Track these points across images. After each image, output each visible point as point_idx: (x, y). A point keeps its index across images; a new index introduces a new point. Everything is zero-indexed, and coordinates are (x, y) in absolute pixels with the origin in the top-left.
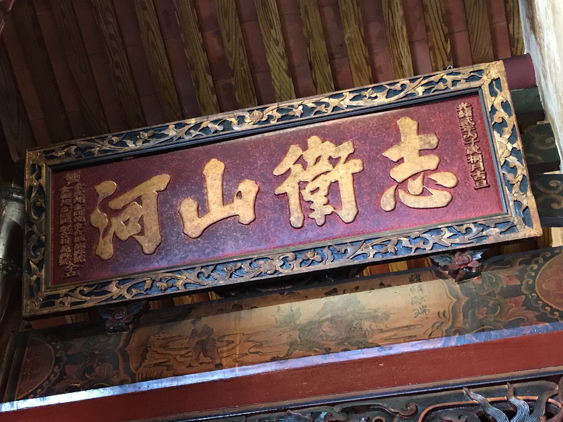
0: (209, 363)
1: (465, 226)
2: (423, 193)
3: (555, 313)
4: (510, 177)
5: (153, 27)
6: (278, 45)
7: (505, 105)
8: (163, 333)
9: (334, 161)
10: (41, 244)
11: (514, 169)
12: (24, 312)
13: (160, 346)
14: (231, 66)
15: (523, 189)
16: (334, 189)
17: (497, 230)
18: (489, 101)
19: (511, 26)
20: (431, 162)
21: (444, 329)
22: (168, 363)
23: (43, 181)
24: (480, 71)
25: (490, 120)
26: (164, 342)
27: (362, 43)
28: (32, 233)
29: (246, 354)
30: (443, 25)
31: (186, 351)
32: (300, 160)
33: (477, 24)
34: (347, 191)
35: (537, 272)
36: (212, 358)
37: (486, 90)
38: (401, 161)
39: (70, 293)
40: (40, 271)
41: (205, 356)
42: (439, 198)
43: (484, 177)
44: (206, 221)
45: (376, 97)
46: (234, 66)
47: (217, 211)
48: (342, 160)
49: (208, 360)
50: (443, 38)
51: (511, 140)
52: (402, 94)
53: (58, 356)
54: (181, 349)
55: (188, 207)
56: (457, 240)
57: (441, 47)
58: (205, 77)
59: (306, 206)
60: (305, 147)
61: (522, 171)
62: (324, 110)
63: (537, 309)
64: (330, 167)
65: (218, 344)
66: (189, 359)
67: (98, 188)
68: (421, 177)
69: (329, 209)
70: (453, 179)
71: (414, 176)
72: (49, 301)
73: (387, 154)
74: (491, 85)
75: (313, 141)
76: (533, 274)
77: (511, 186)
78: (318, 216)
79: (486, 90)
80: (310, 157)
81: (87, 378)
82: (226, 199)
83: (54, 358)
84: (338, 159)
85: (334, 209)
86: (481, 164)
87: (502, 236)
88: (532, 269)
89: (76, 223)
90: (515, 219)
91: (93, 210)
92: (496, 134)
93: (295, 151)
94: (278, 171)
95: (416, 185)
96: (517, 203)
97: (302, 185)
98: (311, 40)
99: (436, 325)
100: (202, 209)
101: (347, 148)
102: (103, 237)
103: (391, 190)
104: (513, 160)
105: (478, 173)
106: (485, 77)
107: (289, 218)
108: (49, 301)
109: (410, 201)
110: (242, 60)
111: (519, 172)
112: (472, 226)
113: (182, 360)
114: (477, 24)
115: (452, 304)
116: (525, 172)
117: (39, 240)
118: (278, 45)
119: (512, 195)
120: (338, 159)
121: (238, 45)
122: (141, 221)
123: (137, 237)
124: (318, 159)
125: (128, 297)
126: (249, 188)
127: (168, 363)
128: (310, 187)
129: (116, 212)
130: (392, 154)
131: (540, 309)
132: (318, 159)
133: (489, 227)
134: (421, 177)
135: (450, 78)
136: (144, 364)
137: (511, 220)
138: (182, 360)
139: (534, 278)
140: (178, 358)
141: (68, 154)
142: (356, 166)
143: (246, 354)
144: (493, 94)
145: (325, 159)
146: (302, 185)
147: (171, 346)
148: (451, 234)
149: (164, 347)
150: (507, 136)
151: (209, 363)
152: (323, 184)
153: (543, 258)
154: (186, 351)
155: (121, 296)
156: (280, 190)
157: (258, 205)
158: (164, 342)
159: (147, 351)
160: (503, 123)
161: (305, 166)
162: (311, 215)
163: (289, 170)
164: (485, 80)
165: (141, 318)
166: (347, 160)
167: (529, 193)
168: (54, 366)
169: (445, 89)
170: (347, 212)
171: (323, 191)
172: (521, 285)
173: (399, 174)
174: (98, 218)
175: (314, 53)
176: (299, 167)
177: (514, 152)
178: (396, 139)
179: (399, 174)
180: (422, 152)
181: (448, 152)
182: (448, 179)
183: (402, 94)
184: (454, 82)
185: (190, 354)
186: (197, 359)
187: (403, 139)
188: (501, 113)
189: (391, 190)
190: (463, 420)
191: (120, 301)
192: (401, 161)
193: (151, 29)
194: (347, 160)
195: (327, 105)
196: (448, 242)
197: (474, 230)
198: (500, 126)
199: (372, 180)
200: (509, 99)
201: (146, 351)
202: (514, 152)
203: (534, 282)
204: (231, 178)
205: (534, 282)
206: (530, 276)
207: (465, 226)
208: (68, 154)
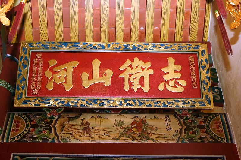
0: (88, 136)
1: (188, 101)
2: (175, 86)
3: (216, 137)
4: (205, 86)
5: (75, 3)
6: (121, 19)
7: (206, 60)
8: (70, 122)
9: (143, 69)
10: (24, 79)
11: (207, 84)
12: (15, 105)
13: (69, 127)
14: (102, 23)
15: (209, 91)
16: (142, 79)
17: (199, 104)
18: (201, 57)
19: (205, 30)
20: (178, 76)
21: (177, 137)
22: (71, 134)
23: (27, 55)
24: (199, 46)
25: (200, 64)
26: (71, 125)
27: (152, 25)
28: (21, 74)
29: (103, 135)
30: (182, 25)
31: (79, 130)
32: (130, 66)
33: (194, 27)
34: (147, 81)
35: (210, 121)
36: (89, 135)
37: (200, 53)
38: (168, 73)
39: (34, 101)
40: (23, 90)
41: (87, 133)
42: (180, 90)
43: (196, 84)
44: (92, 83)
45: (161, 48)
46: (103, 24)
47: (97, 80)
48: (146, 69)
49: (88, 135)
50: (181, 30)
51: (207, 73)
52: (170, 49)
53: (27, 124)
54: (77, 129)
55: (85, 76)
56: (184, 106)
57: (179, 33)
58: (91, 25)
59: (131, 84)
60: (133, 61)
61: (209, 85)
62: (141, 49)
63: (210, 135)
64: (141, 71)
65: (92, 130)
66: (81, 133)
67: (49, 62)
68: (174, 81)
69: (140, 86)
70: (185, 83)
71: (172, 80)
72: (25, 102)
73: (162, 70)
74: (202, 52)
75: (136, 59)
76: (209, 122)
77: (205, 90)
78: (135, 88)
79: (200, 53)
80: (134, 65)
81: (39, 135)
82: (101, 75)
83: (25, 125)
84: (145, 68)
85: (141, 86)
86: (196, 79)
87: (200, 106)
88: (208, 120)
89: (39, 74)
90: (205, 101)
91: (46, 70)
92: (202, 70)
93: (128, 62)
94: (121, 68)
95: (172, 83)
96: (207, 96)
97: (130, 75)
98: (134, 20)
99: (175, 135)
100: (91, 78)
101: (149, 65)
102: (50, 81)
103: (163, 83)
104: (206, 80)
105: (194, 83)
106: (200, 48)
107: (124, 86)
108: (25, 102)
109: (169, 88)
110: (106, 22)
111: (208, 84)
112: (190, 101)
113: (77, 133)
114: (194, 27)
115: (180, 128)
116: (210, 85)
117: (24, 78)
118: (121, 19)
119: (205, 93)
120: (145, 68)
121: (106, 16)
122: (65, 78)
123: (63, 84)
124: (137, 67)
125: (58, 106)
126: (109, 73)
127: (71, 134)
128: (133, 77)
129: (56, 73)
130: (165, 70)
131: (211, 135)
132: (137, 67)
133: (196, 103)
134: (174, 81)
135: (188, 46)
136: (62, 133)
137: (204, 102)
138: (77, 133)
139: (209, 123)
140: (76, 132)
141: (39, 46)
142: (151, 72)
143: (103, 135)
144: (203, 55)
145: (139, 67)
146: (130, 75)
147: (73, 127)
148: (183, 103)
149: (71, 127)
150: (206, 71)
151: (88, 136)
152: (138, 77)
153: (212, 116)
154: (79, 130)
155: (55, 106)
156: (121, 76)
157: (113, 80)
158: (71, 125)
159: (64, 128)
160: (205, 67)
161: (132, 68)
162: (132, 87)
163: (126, 69)
164: (200, 49)
165: (61, 115)
166: (148, 69)
167: (24, 12)
168: (26, 128)
169: (186, 50)
170: (146, 89)
171: (138, 79)
172: (205, 125)
173: (166, 78)
174: (48, 74)
175: (134, 25)
176: (130, 68)
177: (207, 77)
178: (166, 65)
179: (166, 78)
180: (176, 72)
181: (185, 74)
182: (183, 83)
183: (170, 49)
184: (189, 48)
185: (81, 132)
186: (84, 134)
187: (169, 65)
188: (204, 63)
189: (163, 83)
190: (6, 22)
191: (54, 107)
192: (168, 73)
193: (74, 4)
194: (148, 69)
195: (142, 47)
196: (181, 106)
197: (191, 103)
198: (204, 67)
199: (157, 78)
200: (208, 58)
201: (63, 128)
202: (207, 77)
203: (209, 124)
204: (103, 67)
205: (209, 124)
206: (208, 122)
207: (188, 101)
208: (39, 46)
